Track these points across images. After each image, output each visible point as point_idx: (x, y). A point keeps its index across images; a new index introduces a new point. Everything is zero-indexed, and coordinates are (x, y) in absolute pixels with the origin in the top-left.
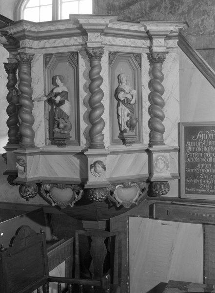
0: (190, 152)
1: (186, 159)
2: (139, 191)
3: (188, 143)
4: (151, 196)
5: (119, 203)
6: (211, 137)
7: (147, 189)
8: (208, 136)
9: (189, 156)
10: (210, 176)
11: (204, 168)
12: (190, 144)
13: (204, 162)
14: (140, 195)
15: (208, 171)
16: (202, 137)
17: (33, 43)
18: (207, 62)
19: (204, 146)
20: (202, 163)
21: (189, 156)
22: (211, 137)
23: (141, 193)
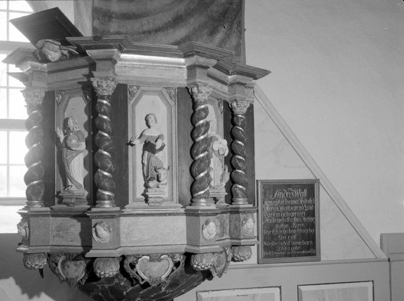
0: (268, 213)
1: (264, 220)
2: (172, 265)
3: (266, 203)
4: (264, 248)
5: (143, 280)
6: (289, 196)
7: (182, 262)
8: (285, 194)
9: (267, 216)
10: (287, 237)
11: (281, 229)
12: (268, 204)
13: (281, 223)
14: (173, 270)
15: (286, 232)
16: (299, 195)
17: (79, 92)
18: (201, 79)
19: (281, 206)
20: (279, 224)
21: (267, 216)
22: (289, 196)
23: (175, 268)
